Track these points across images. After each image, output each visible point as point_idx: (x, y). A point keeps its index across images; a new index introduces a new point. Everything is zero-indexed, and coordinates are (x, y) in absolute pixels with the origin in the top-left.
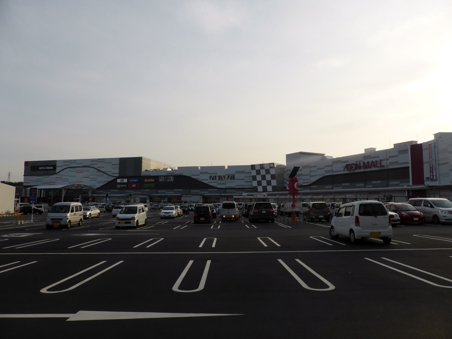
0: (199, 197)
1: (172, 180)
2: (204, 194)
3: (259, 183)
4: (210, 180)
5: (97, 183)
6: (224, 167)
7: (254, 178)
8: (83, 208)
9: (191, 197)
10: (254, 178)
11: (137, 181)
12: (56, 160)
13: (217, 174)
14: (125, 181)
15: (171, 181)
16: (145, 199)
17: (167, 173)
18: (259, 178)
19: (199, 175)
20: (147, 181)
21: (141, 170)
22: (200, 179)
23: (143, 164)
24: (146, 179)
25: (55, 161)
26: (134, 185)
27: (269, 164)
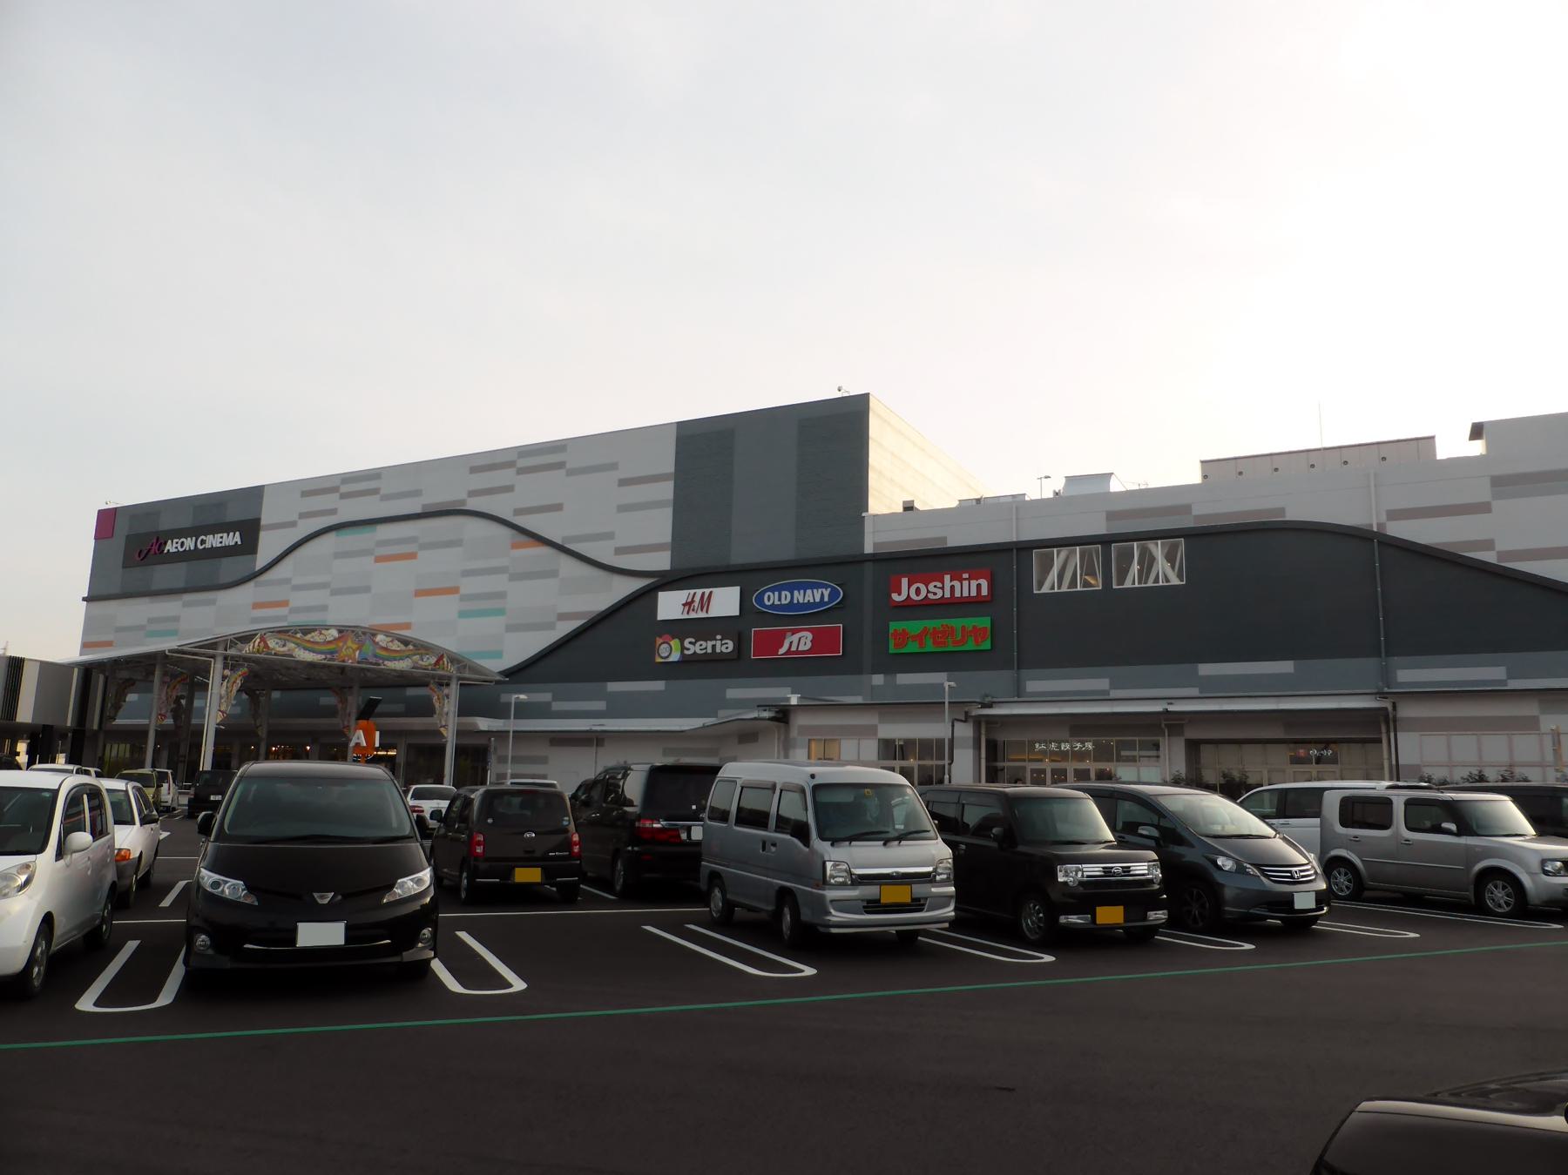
5: (511, 628)
8: (944, 759)
9: (1531, 724)
12: (262, 487)
14: (725, 601)
17: (1112, 516)
19: (1484, 508)
20: (918, 591)
21: (864, 505)
22: (1501, 546)
24: (905, 581)
25: (254, 495)
26: (795, 638)
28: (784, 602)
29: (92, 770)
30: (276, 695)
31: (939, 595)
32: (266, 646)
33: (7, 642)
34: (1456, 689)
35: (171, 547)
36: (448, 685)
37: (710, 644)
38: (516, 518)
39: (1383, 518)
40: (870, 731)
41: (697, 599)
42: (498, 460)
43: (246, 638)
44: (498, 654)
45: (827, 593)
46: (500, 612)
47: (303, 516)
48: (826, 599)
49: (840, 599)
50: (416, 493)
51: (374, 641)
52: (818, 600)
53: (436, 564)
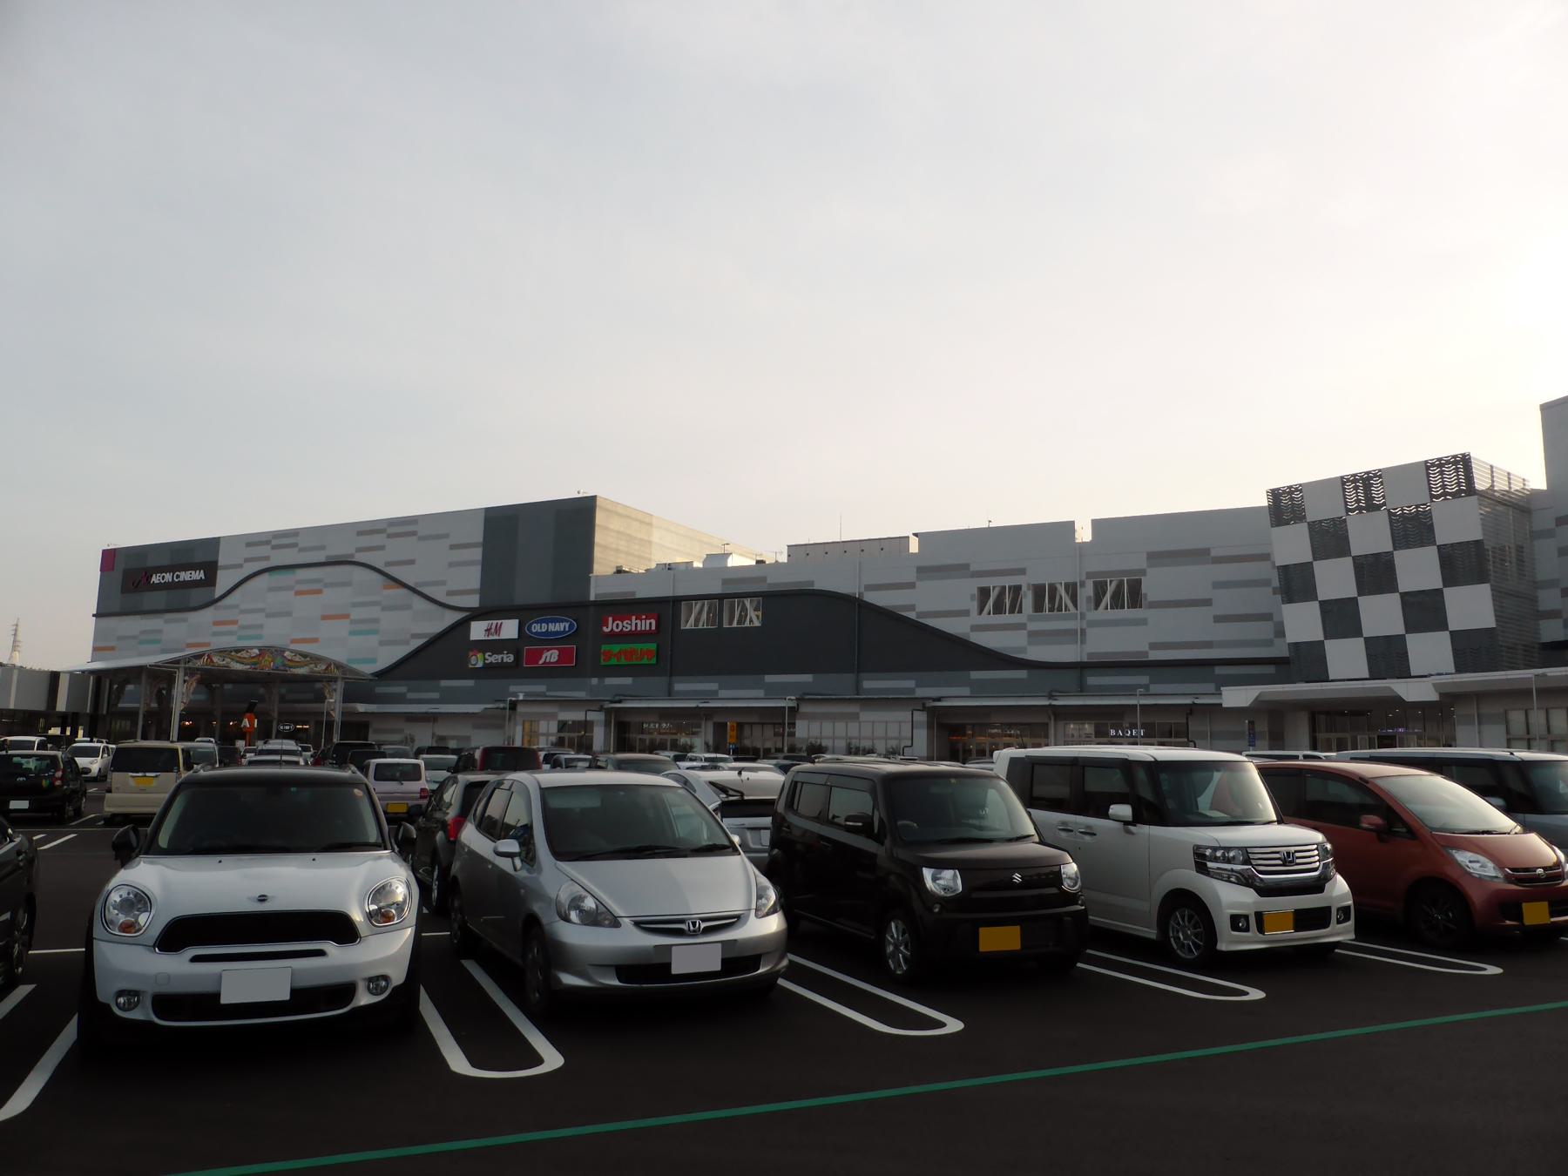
0: (903, 715)
1: (754, 619)
2: (939, 699)
3: (1341, 618)
4: (981, 611)
5: (382, 643)
6: (1069, 527)
7: (1296, 584)
9: (855, 717)
10: (1296, 584)
11: (564, 631)
13: (1022, 572)
14: (510, 629)
15: (747, 624)
16: (587, 725)
17: (725, 582)
18: (1335, 579)
19: (911, 586)
21: (590, 569)
23: (599, 537)
24: (610, 619)
25: (214, 543)
27: (1427, 466)
28: (544, 630)
29: (104, 741)
30: (228, 687)
31: (629, 629)
32: (212, 661)
33: (18, 619)
34: (876, 697)
35: (155, 579)
36: (335, 681)
37: (500, 656)
38: (388, 568)
39: (862, 590)
40: (553, 716)
41: (494, 627)
42: (378, 527)
43: (198, 656)
44: (374, 661)
45: (567, 625)
46: (375, 632)
47: (247, 560)
48: (567, 629)
49: (575, 629)
50: (322, 548)
51: (283, 656)
52: (562, 629)
53: (334, 598)
